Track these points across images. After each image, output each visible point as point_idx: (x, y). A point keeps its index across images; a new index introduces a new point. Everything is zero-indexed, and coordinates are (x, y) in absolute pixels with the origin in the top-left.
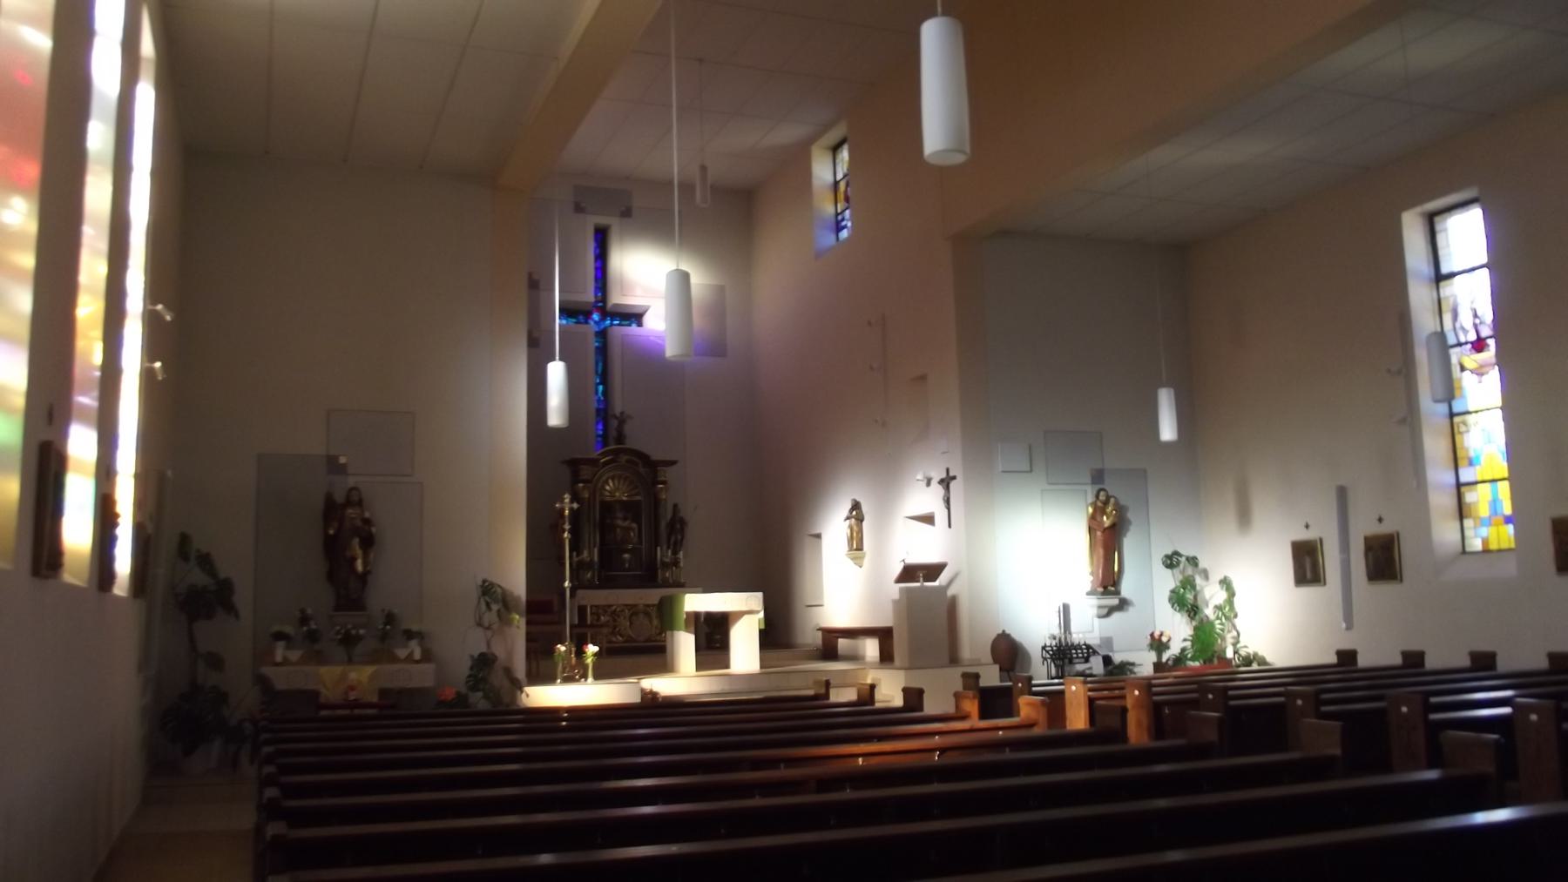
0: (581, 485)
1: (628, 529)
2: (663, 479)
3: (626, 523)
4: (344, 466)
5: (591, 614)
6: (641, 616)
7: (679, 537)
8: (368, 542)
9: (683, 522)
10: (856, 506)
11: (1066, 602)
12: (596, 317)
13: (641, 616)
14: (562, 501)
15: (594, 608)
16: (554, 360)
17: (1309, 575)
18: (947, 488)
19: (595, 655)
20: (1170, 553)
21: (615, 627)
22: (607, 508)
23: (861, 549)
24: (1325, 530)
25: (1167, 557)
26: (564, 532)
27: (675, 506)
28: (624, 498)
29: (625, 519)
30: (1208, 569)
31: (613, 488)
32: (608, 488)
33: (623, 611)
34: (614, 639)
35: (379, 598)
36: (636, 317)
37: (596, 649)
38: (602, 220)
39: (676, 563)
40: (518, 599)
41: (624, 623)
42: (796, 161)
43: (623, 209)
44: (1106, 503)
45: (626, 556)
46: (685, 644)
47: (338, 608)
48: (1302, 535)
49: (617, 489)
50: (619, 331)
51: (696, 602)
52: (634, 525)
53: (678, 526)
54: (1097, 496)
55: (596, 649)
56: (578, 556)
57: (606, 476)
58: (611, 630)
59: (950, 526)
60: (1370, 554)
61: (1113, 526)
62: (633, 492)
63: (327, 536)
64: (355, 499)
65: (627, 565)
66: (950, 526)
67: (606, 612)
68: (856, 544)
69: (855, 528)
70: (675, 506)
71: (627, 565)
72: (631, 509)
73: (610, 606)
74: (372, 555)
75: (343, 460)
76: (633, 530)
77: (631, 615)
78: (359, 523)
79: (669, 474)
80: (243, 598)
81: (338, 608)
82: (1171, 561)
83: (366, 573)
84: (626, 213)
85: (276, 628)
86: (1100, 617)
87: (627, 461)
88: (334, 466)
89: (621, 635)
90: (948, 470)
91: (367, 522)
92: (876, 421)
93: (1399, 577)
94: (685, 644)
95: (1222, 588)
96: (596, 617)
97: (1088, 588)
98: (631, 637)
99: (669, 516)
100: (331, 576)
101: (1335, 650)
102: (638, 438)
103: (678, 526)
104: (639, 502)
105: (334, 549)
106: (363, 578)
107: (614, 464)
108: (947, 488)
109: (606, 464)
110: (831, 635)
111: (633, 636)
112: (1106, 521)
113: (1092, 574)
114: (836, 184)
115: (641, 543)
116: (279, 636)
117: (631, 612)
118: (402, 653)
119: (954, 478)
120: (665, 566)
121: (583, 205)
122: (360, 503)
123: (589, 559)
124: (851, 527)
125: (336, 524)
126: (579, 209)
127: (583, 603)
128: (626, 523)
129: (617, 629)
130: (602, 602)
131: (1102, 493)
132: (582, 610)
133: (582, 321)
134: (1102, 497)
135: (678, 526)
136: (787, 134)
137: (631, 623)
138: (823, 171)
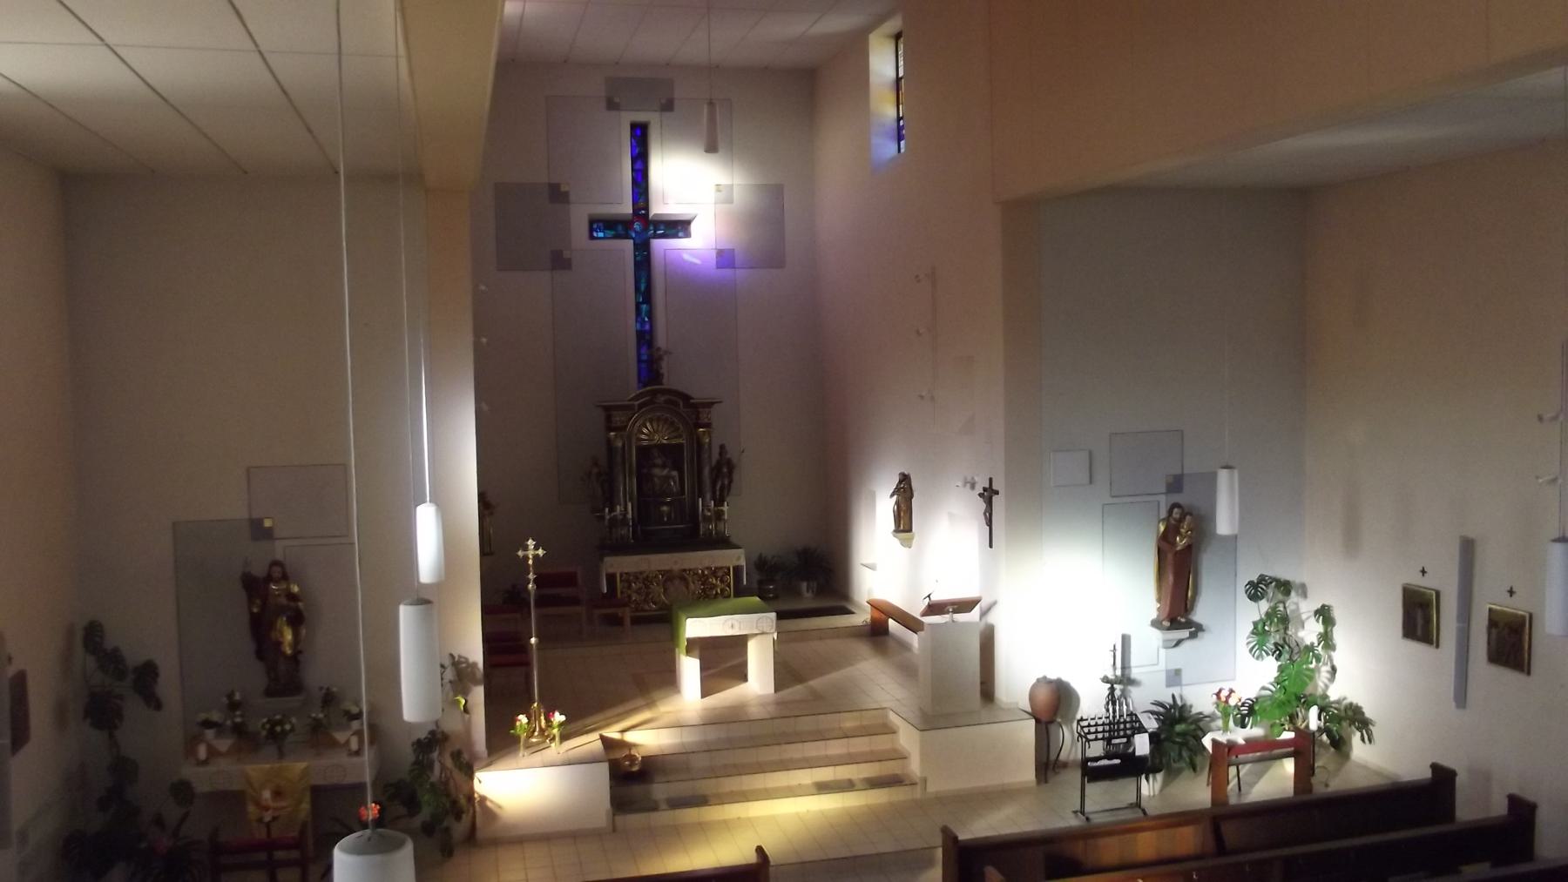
0: (612, 434)
1: (667, 478)
2: (706, 420)
3: (665, 472)
4: (270, 529)
5: (621, 581)
6: (677, 582)
7: (726, 482)
8: (297, 620)
9: (731, 466)
10: (905, 479)
11: (1127, 632)
12: (637, 226)
13: (677, 582)
14: (526, 548)
15: (625, 575)
16: (424, 502)
17: (1419, 632)
18: (989, 503)
19: (561, 724)
20: (1255, 578)
21: (648, 594)
22: (645, 452)
23: (910, 530)
24: (1443, 580)
25: (1251, 583)
26: (529, 583)
27: (722, 447)
28: (665, 442)
29: (664, 466)
30: (1307, 585)
31: (649, 432)
32: (645, 431)
33: (656, 576)
34: (646, 607)
35: (317, 675)
36: (678, 227)
37: (563, 718)
38: (640, 117)
39: (719, 516)
40: (475, 665)
41: (656, 589)
42: (853, 49)
43: (663, 101)
44: (1181, 520)
45: (665, 508)
46: (689, 669)
47: (269, 693)
48: (1416, 580)
49: (656, 432)
50: (661, 246)
51: (696, 627)
52: (675, 473)
53: (725, 470)
54: (1170, 512)
55: (563, 718)
56: (610, 512)
57: (638, 424)
58: (643, 598)
59: (991, 546)
60: (1494, 631)
61: (1189, 548)
62: (675, 434)
63: (252, 614)
64: (280, 571)
65: (665, 519)
66: (991, 546)
67: (637, 578)
68: (904, 522)
69: (903, 506)
70: (722, 447)
71: (665, 519)
72: (672, 454)
73: (641, 573)
74: (303, 632)
75: (268, 523)
76: (673, 478)
77: (665, 581)
78: (283, 601)
79: (715, 415)
80: (168, 686)
81: (269, 693)
82: (1255, 591)
83: (297, 653)
84: (668, 106)
85: (203, 716)
86: (1166, 647)
87: (666, 402)
88: (259, 532)
89: (655, 603)
90: (991, 480)
91: (293, 597)
92: (922, 397)
93: (1526, 669)
94: (689, 669)
95: (1317, 621)
96: (626, 585)
97: (1154, 615)
98: (666, 605)
99: (715, 456)
100: (260, 654)
101: (1430, 763)
102: (676, 376)
103: (725, 470)
104: (682, 444)
105: (261, 628)
106: (295, 658)
107: (652, 406)
108: (989, 503)
109: (641, 406)
110: (884, 612)
111: (666, 602)
112: (1181, 543)
113: (1159, 600)
114: (898, 80)
115: (683, 493)
116: (208, 724)
117: (665, 578)
118: (340, 737)
119: (997, 493)
120: (708, 520)
121: (617, 100)
122: (285, 577)
123: (621, 517)
124: (897, 503)
125: (258, 602)
126: (612, 105)
127: (611, 571)
128: (665, 472)
129: (650, 596)
130: (632, 570)
131: (1176, 510)
132: (611, 578)
133: (623, 232)
134: (1176, 513)
135: (725, 470)
136: (837, 23)
137: (665, 590)
138: (883, 64)
